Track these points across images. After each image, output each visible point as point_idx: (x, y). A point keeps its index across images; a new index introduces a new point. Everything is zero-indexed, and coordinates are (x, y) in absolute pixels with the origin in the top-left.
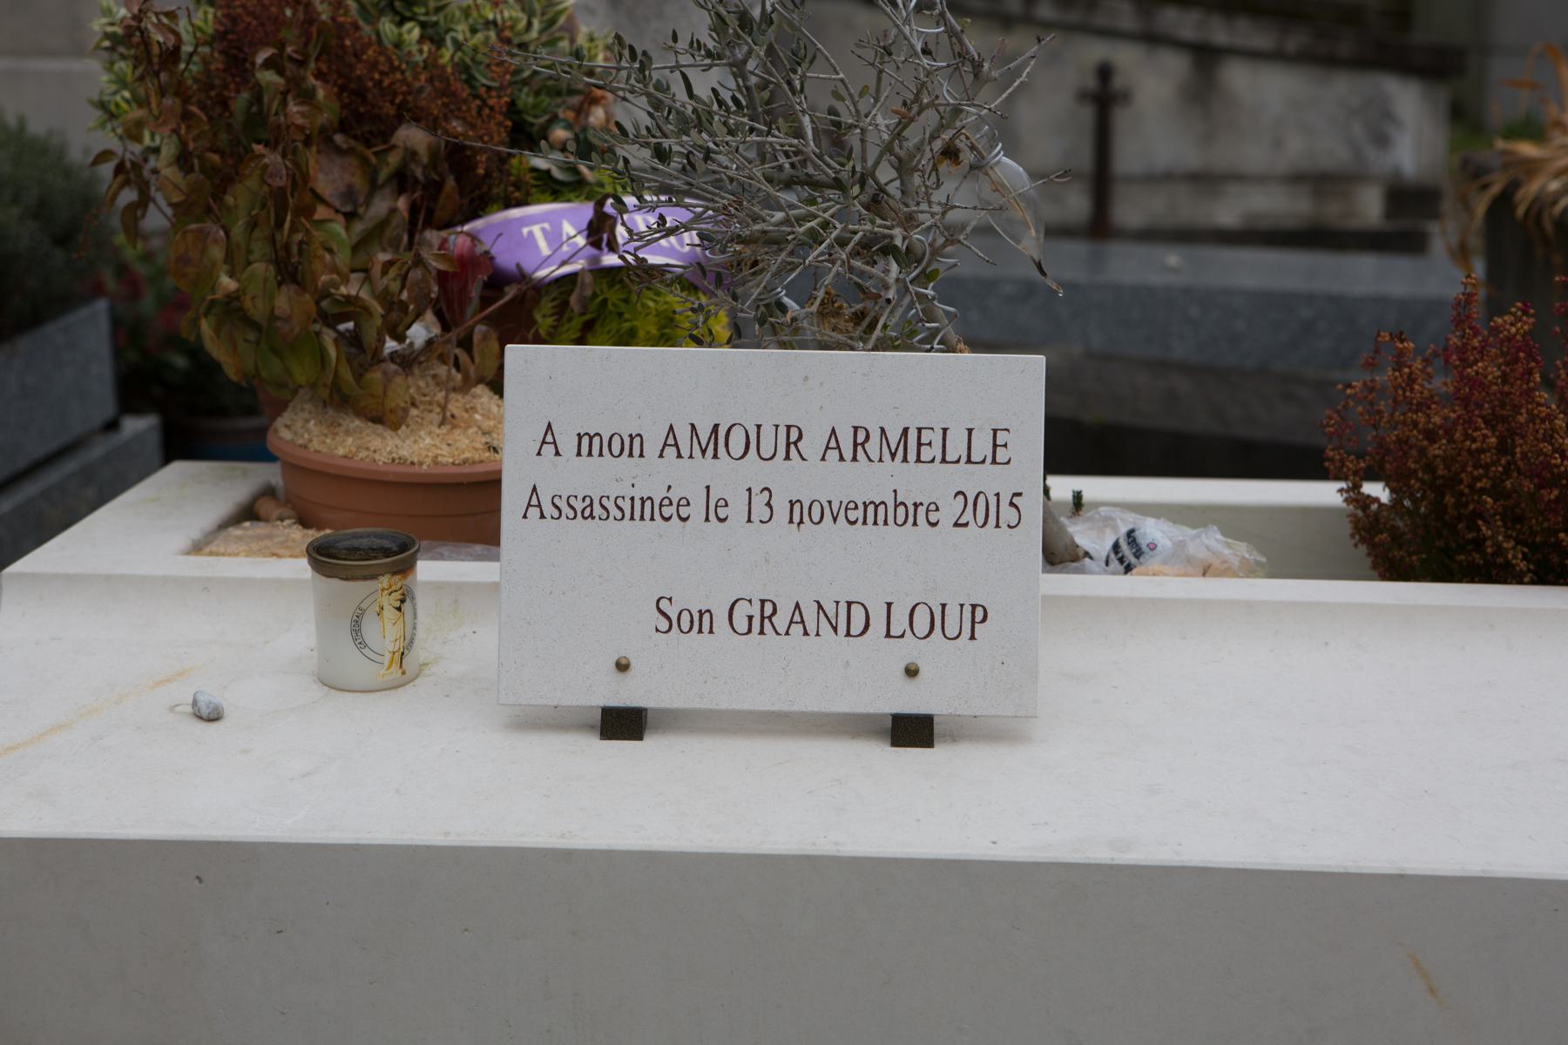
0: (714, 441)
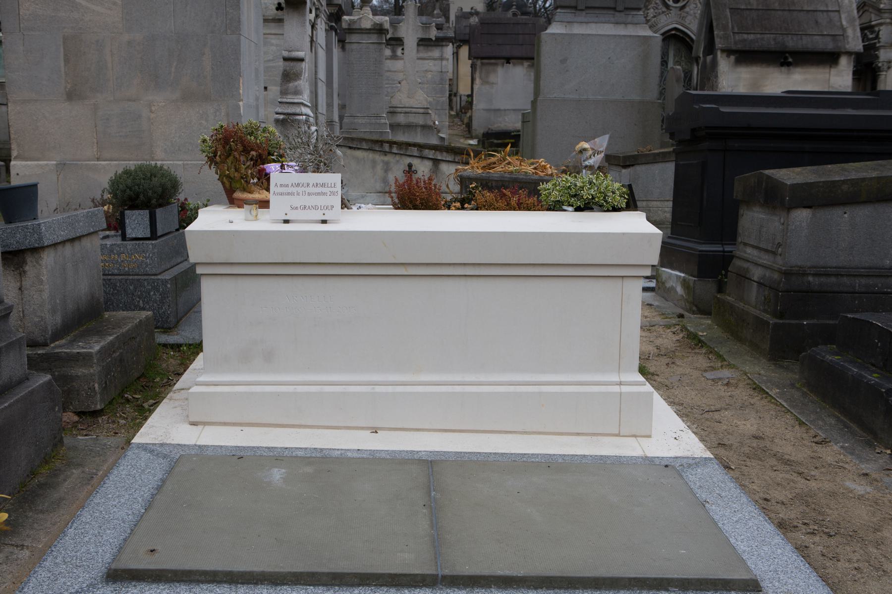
0: (298, 185)
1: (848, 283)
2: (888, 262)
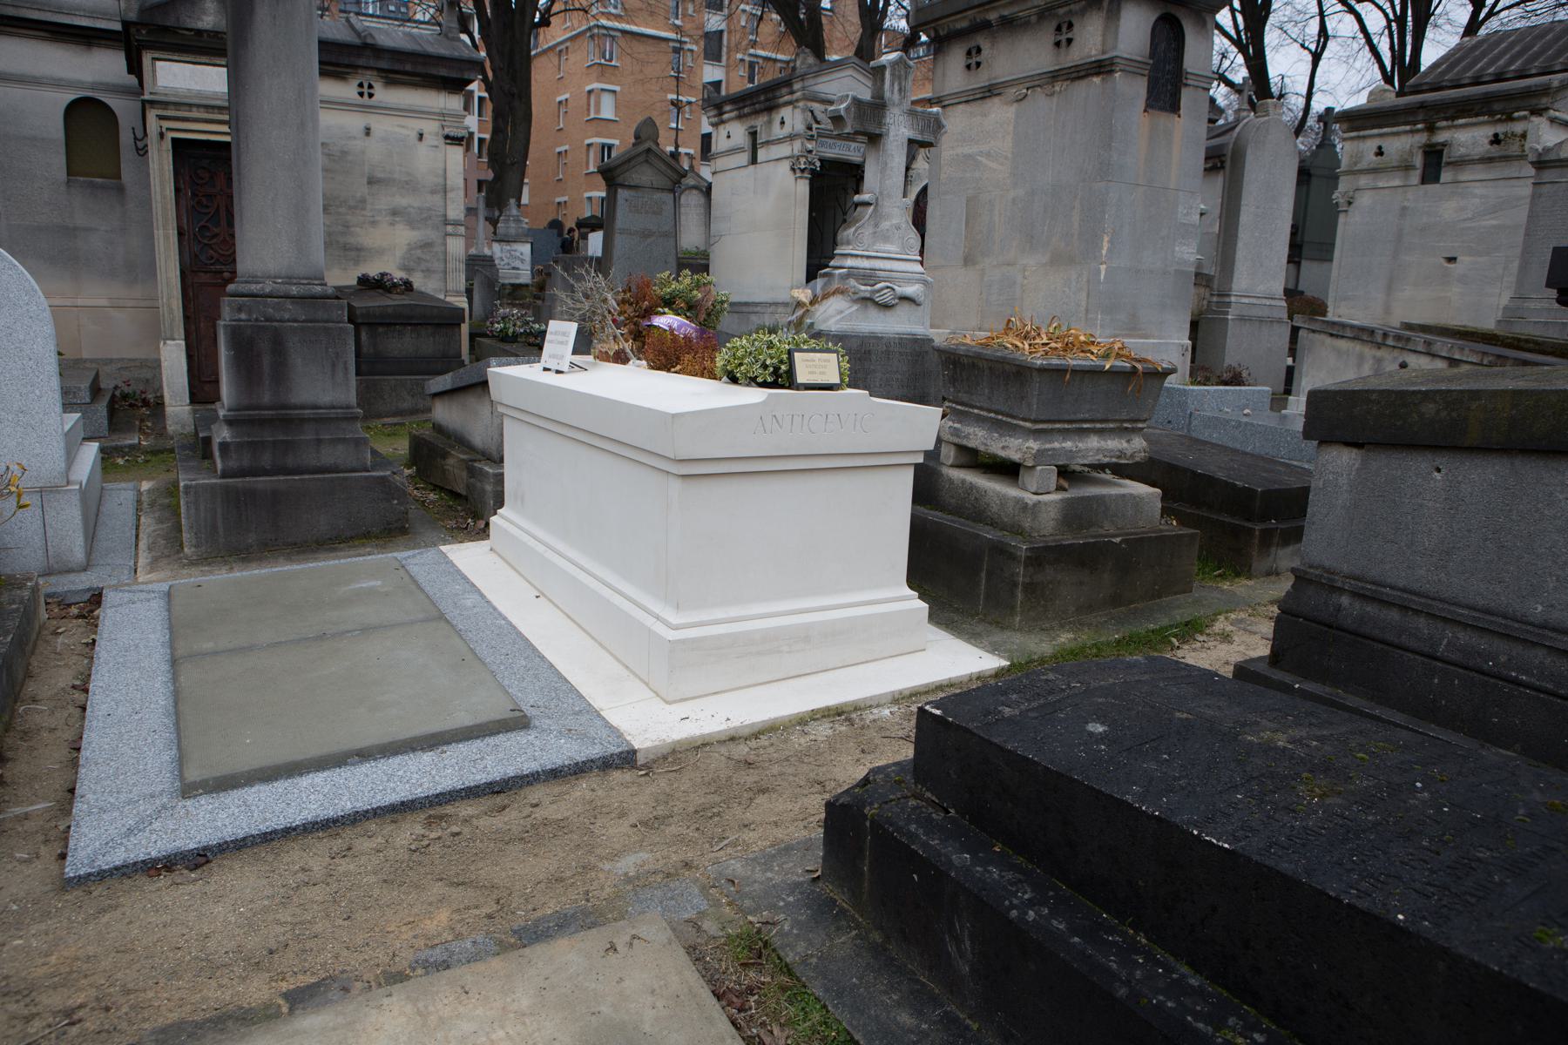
1: (1426, 631)
2: (1540, 608)
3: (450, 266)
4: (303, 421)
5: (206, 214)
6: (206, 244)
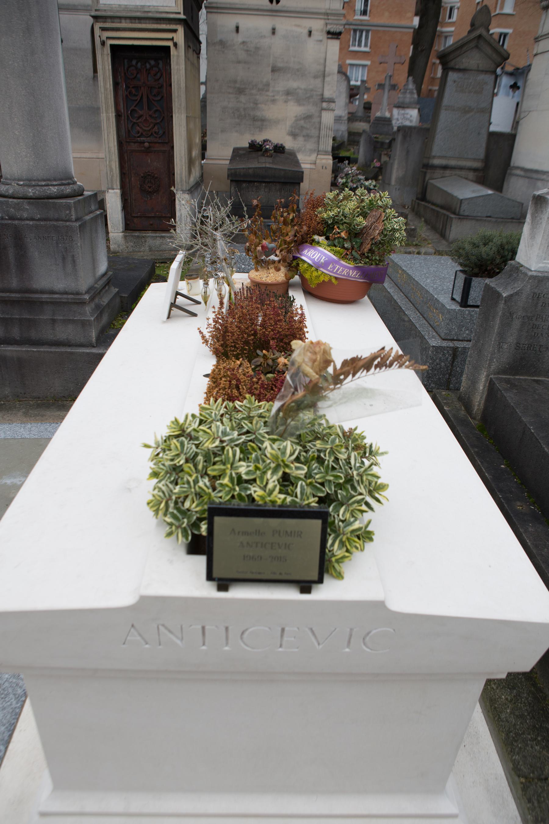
3: (323, 133)
4: (42, 303)
5: (136, 100)
6: (134, 123)
